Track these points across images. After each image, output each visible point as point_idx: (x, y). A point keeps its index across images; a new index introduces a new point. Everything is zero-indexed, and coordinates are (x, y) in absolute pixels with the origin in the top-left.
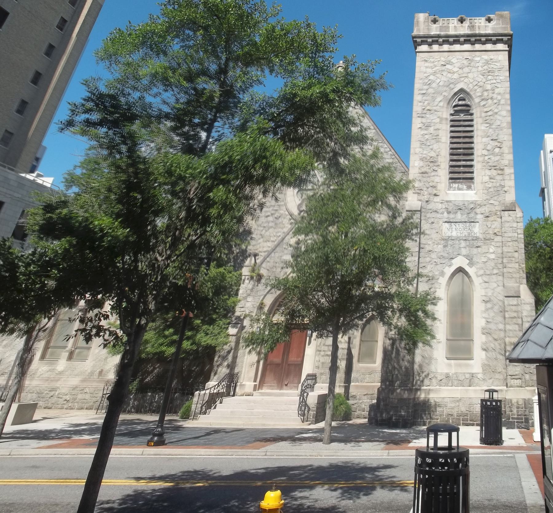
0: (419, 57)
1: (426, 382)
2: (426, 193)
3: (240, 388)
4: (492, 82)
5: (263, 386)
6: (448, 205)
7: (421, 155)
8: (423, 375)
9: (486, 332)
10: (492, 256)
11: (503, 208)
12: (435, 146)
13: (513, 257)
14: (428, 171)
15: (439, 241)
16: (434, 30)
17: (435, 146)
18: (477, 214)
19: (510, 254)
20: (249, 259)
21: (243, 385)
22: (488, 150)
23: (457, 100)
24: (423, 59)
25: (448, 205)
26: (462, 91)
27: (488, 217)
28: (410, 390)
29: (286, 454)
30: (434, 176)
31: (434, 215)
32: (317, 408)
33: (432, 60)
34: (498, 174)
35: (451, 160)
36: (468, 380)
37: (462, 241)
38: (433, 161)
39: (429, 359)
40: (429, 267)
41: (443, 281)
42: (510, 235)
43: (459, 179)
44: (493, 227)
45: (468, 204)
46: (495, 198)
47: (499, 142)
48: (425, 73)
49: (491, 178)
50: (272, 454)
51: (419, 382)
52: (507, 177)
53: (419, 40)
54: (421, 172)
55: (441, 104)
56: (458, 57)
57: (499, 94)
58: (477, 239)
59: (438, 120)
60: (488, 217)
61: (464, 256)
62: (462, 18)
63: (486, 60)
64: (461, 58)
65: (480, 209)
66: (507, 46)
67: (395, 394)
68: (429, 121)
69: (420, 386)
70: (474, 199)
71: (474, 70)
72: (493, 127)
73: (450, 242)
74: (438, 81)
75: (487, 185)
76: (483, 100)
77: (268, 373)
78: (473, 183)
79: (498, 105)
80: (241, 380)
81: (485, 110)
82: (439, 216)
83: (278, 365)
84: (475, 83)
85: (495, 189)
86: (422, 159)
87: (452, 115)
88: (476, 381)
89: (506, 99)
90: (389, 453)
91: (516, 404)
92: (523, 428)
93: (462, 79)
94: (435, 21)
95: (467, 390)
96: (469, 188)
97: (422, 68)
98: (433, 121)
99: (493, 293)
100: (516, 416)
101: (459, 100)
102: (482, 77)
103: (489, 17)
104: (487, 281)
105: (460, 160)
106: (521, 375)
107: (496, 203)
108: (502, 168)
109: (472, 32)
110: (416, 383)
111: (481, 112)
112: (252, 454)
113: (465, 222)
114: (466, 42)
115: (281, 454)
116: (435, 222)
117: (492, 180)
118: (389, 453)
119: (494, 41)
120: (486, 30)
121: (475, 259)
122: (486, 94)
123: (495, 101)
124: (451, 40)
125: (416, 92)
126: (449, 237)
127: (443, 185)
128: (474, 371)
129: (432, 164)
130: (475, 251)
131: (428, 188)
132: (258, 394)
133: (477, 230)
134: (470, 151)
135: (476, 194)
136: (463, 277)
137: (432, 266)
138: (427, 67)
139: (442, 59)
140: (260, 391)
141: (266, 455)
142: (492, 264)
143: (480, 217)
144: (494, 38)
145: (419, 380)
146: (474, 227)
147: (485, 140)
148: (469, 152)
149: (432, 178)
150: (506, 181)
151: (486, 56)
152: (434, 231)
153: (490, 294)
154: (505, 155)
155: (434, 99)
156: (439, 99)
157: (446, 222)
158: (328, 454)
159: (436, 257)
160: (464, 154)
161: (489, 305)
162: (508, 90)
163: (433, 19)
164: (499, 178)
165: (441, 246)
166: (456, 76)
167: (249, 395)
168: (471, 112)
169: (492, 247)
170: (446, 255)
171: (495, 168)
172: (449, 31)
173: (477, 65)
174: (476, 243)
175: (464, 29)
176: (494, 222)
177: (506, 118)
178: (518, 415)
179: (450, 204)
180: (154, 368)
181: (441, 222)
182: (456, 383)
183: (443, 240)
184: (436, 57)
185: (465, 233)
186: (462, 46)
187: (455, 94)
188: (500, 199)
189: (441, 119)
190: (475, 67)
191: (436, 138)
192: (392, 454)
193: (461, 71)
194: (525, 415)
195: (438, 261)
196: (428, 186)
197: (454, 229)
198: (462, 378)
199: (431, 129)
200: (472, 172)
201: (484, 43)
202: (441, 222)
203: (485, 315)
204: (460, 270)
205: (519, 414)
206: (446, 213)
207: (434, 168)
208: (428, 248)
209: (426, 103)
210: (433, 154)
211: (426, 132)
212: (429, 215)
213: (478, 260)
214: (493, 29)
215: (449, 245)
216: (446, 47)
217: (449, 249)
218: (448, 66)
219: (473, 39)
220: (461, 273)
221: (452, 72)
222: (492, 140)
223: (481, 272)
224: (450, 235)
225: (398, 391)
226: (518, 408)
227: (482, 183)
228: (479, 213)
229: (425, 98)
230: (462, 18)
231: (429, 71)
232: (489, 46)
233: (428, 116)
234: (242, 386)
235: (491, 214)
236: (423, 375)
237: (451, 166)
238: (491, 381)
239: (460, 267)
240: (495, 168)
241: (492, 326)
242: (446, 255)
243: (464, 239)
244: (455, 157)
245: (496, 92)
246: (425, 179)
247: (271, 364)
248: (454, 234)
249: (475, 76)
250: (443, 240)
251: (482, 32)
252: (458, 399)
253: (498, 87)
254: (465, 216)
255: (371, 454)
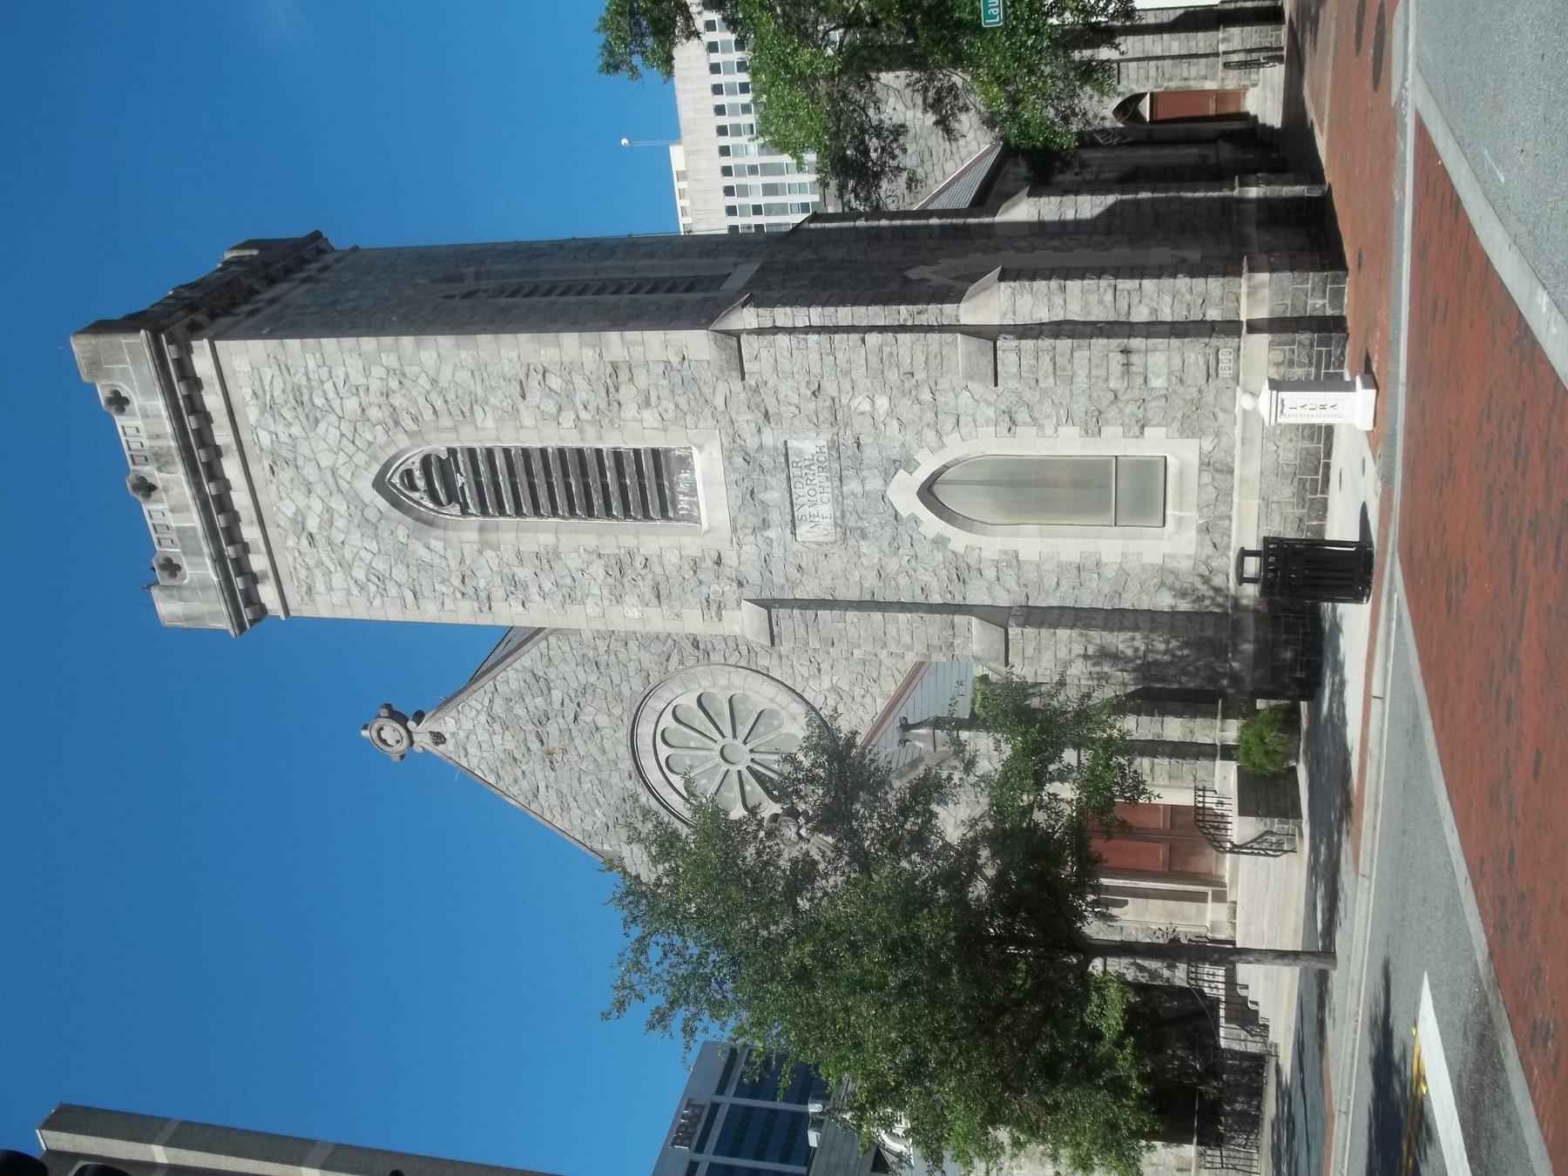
0: (301, 607)
1: (1218, 581)
2: (715, 587)
3: (1219, 932)
4: (331, 395)
5: (1216, 876)
6: (744, 526)
7: (606, 602)
8: (1203, 589)
9: (1094, 423)
10: (882, 403)
11: (736, 374)
12: (574, 562)
13: (881, 350)
14: (649, 582)
15: (851, 551)
16: (201, 570)
17: (574, 562)
18: (761, 445)
19: (874, 360)
20: (907, 761)
21: (1212, 926)
22: (560, 409)
23: (416, 495)
24: (306, 598)
25: (744, 526)
26: (380, 484)
27: (766, 415)
28: (1237, 631)
29: (1347, 1075)
30: (662, 566)
31: (777, 565)
32: (1266, 815)
33: (303, 574)
34: (631, 379)
35: (608, 512)
36: (1218, 476)
37: (845, 489)
38: (619, 567)
39: (1165, 576)
40: (925, 577)
41: (959, 539)
42: (815, 357)
43: (660, 488)
44: (795, 399)
45: (735, 470)
46: (707, 390)
47: (527, 376)
48: (348, 591)
49: (648, 404)
50: (1344, 1101)
51: (1220, 600)
52: (637, 353)
53: (247, 614)
54: (655, 601)
55: (437, 545)
56: (274, 498)
57: (366, 371)
58: (834, 446)
59: (489, 554)
60: (766, 415)
61: (886, 483)
62: (136, 487)
63: (262, 413)
64: (273, 487)
65: (747, 436)
66: (194, 343)
67: (1243, 674)
68: (498, 581)
69: (1227, 596)
70: (717, 455)
71: (304, 448)
72: (480, 391)
73: (852, 521)
74: (367, 556)
75: (670, 415)
76: (397, 423)
77: (1191, 869)
78: (667, 451)
79: (404, 374)
80: (1203, 931)
81: (428, 415)
82: (778, 552)
83: (1172, 850)
84: (351, 449)
85: (678, 390)
86: (619, 599)
87: (464, 511)
88: (1219, 455)
89: (380, 350)
90: (1364, 876)
91: (1282, 370)
92: (1342, 354)
93: (343, 484)
94: (172, 568)
95: (1243, 482)
96: (685, 462)
97: (335, 601)
98: (495, 568)
99: (988, 404)
100: (1313, 370)
101: (413, 488)
102: (322, 426)
103: (110, 401)
104: (954, 420)
105: (605, 487)
106: (1208, 350)
107: (722, 388)
108: (609, 370)
109: (178, 459)
110: (1219, 605)
111: (438, 429)
112: (1342, 1137)
113: (789, 479)
114: (215, 473)
115: (1346, 1086)
116: (797, 561)
117: (653, 400)
118: (1364, 876)
119: (189, 387)
120: (159, 416)
121: (895, 453)
122: (374, 413)
123: (394, 384)
124: (220, 521)
125: (412, 615)
126: (836, 524)
127: (686, 540)
128: (1195, 460)
129: (630, 574)
130: (870, 453)
131: (700, 582)
132: (1234, 892)
133: (809, 445)
134: (572, 461)
135: (700, 448)
136: (942, 483)
137: (920, 569)
138: (330, 588)
139: (291, 542)
140: (1227, 881)
141: (1347, 1113)
142: (905, 406)
143: (769, 438)
144: (181, 389)
145: (1213, 599)
146: (800, 453)
147: (528, 420)
148: (576, 462)
149: (670, 570)
150: (651, 356)
151: (250, 414)
152: (822, 564)
153: (991, 413)
154: (566, 359)
155: (424, 566)
156: (424, 553)
157: (794, 533)
158: (1355, 999)
159: (895, 559)
160: (584, 473)
161: (1022, 415)
162: (348, 342)
163: (166, 574)
164: (642, 378)
165: (865, 547)
166: (339, 505)
167: (1235, 912)
168: (444, 456)
169: (855, 403)
170: (888, 532)
171: (612, 390)
172: (194, 529)
173: (284, 438)
174: (848, 449)
175: (175, 482)
176: (782, 397)
177: (442, 352)
178: (1310, 364)
179: (741, 520)
180: (1175, 1057)
181: (796, 546)
182: (1222, 509)
183: (845, 539)
184: (291, 560)
185: (820, 478)
186: (233, 484)
187: (395, 503)
188: (707, 374)
189: (484, 546)
190: (295, 446)
191: (547, 559)
192: (1368, 870)
193: (319, 489)
194: (1312, 345)
195: (905, 550)
196: (693, 583)
197: (813, 511)
198: (1210, 493)
199: (523, 573)
200: (637, 452)
201: (205, 418)
202: (796, 546)
203: (1049, 425)
204: (927, 493)
205: (1306, 361)
206: (767, 533)
207: (638, 564)
208: (871, 581)
209: (439, 587)
210: (598, 569)
211: (534, 590)
212: (778, 578)
213: (897, 444)
214: (147, 392)
215: (860, 524)
216: (250, 533)
217: (870, 525)
218: (312, 524)
219: (201, 455)
220: (937, 488)
221: (326, 516)
222: (524, 397)
223: (930, 436)
224: (831, 521)
225: (1236, 665)
226: (1291, 363)
227: (666, 430)
228: (756, 440)
229: (427, 592)
230: (136, 487)
231: (338, 579)
232: (212, 400)
233: (482, 584)
234: (1214, 927)
235: (758, 406)
236: (1203, 589)
237: (626, 512)
238: (1221, 416)
239: (919, 494)
240: (612, 390)
241: (1080, 405)
242: (888, 532)
243: (837, 483)
244: (597, 501)
245: (363, 381)
246: (676, 591)
247: (1170, 862)
248: (826, 509)
249: (322, 445)
250: (845, 539)
251: (168, 427)
252: (1263, 505)
253: (347, 375)
254: (772, 481)
255: (1363, 914)
